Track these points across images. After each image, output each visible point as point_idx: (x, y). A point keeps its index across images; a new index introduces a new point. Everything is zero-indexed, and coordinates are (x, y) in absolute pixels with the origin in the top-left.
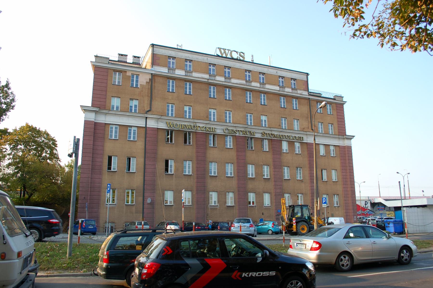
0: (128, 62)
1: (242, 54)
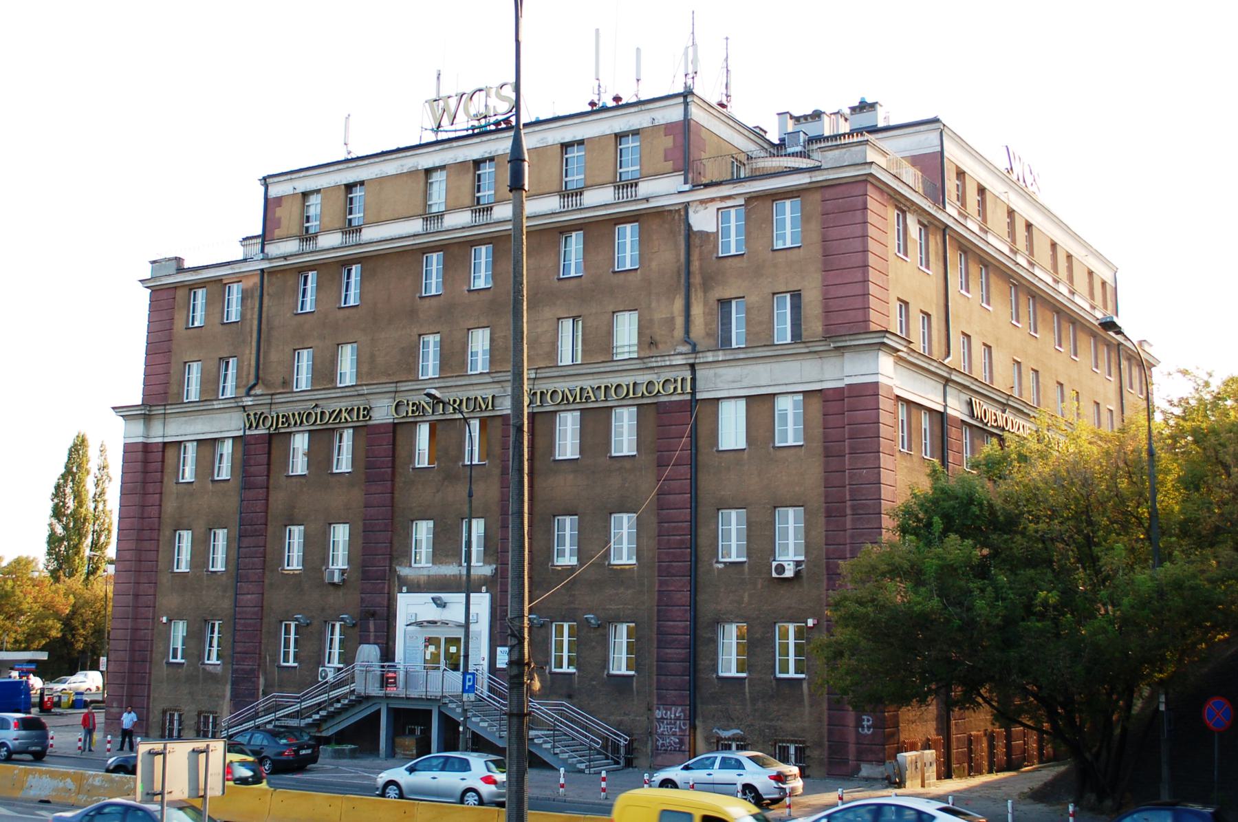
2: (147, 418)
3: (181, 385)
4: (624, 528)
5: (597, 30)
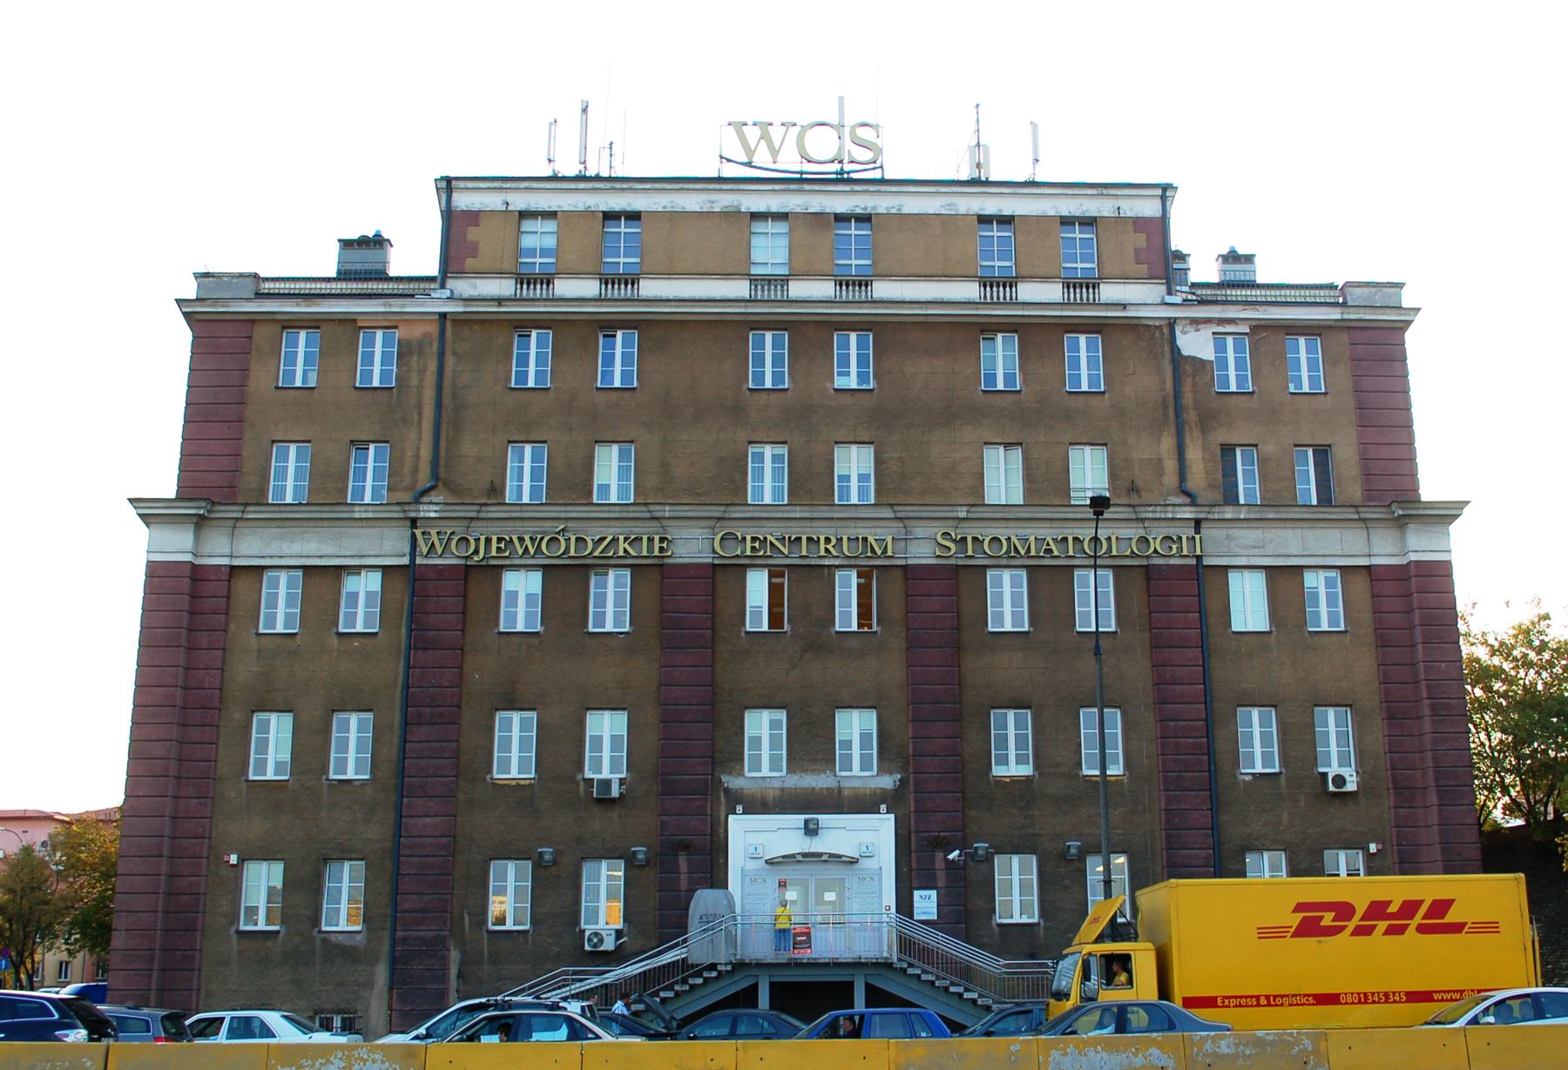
0: (1259, 281)
1: (864, 133)
3: (265, 477)
4: (607, 729)
5: (841, 99)
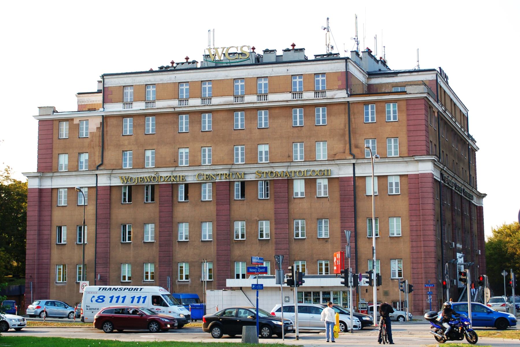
2: (40, 178)
